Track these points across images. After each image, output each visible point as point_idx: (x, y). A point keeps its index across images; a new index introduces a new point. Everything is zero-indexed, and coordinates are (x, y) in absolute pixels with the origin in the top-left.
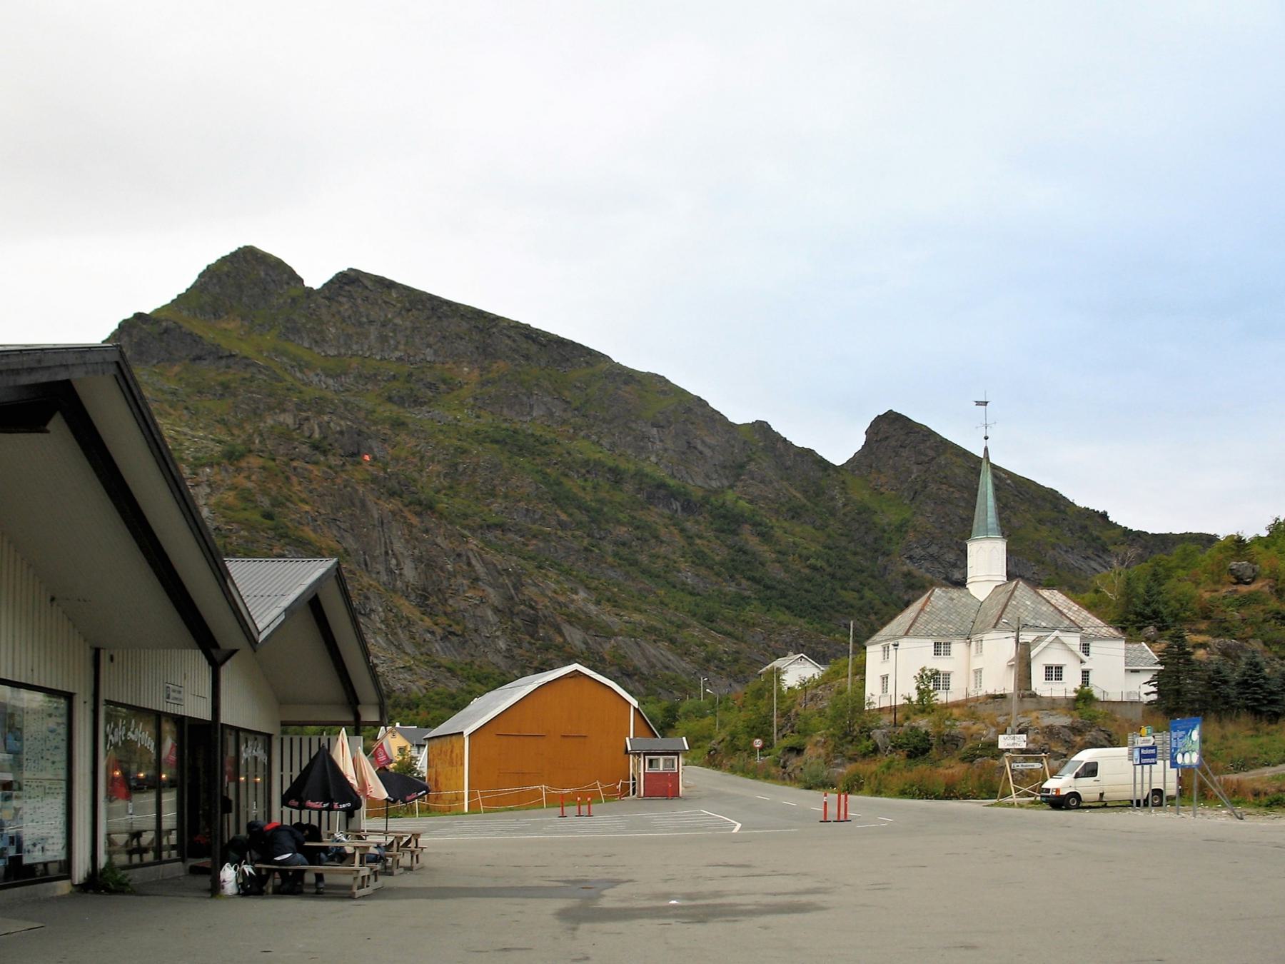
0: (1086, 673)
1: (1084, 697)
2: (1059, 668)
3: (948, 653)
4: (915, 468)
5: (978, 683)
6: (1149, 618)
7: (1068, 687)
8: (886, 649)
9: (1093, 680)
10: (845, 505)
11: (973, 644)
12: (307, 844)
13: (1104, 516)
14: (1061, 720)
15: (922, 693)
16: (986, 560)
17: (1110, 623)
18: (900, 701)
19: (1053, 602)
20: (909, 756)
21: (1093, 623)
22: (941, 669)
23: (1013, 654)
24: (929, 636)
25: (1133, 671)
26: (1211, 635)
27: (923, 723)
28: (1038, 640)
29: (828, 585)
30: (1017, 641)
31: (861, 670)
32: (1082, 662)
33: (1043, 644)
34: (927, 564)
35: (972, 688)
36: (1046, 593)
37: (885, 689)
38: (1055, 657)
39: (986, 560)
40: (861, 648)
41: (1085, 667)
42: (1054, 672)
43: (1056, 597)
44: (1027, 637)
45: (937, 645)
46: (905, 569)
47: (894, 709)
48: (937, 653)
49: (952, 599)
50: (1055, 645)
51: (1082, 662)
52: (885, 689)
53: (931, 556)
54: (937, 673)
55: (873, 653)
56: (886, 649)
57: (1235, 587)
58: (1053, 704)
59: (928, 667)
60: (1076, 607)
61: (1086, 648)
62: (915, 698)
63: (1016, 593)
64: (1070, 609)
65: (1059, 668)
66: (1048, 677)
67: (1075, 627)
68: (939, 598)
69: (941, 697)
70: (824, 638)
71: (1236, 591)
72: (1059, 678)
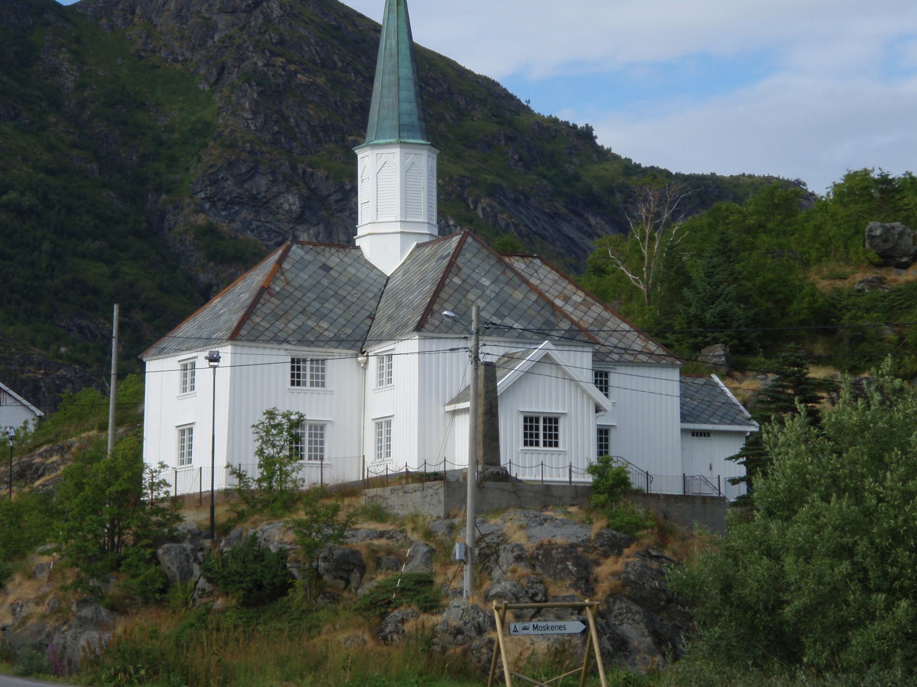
0: (603, 434)
1: (610, 485)
2: (552, 422)
3: (319, 382)
4: (222, 21)
5: (384, 447)
6: (715, 327)
7: (568, 461)
8: (189, 369)
9: (614, 450)
10: (81, 87)
11: (373, 361)
12: (116, 307)
13: (587, 135)
14: (564, 530)
15: (268, 463)
16: (391, 197)
17: (647, 332)
18: (222, 482)
19: (534, 281)
20: (245, 603)
21: (620, 331)
22: (311, 416)
23: (469, 380)
24: (278, 340)
25: (696, 433)
26: (838, 367)
27: (276, 534)
28: (510, 359)
29: (46, 246)
30: (476, 359)
31: (132, 417)
32: (598, 409)
33: (522, 365)
34: (245, 214)
35: (370, 457)
36: (519, 264)
37: (186, 455)
38: (543, 398)
39: (391, 197)
40: (134, 371)
41: (604, 421)
42: (542, 430)
43: (545, 277)
44: (492, 351)
45: (296, 364)
46: (201, 219)
47: (208, 500)
48: (296, 380)
49: (326, 268)
50: (547, 369)
51: (598, 409)
52: (186, 455)
53: (254, 198)
54: (299, 423)
55: (161, 374)
56: (189, 369)
57: (881, 273)
58: (547, 495)
59: (282, 409)
60: (579, 297)
61: (602, 381)
62: (254, 472)
63: (460, 261)
64: (567, 299)
65: (552, 422)
66: (530, 439)
67: (576, 336)
68: (302, 264)
69: (307, 474)
70: (36, 353)
71: (881, 281)
72: (552, 440)
